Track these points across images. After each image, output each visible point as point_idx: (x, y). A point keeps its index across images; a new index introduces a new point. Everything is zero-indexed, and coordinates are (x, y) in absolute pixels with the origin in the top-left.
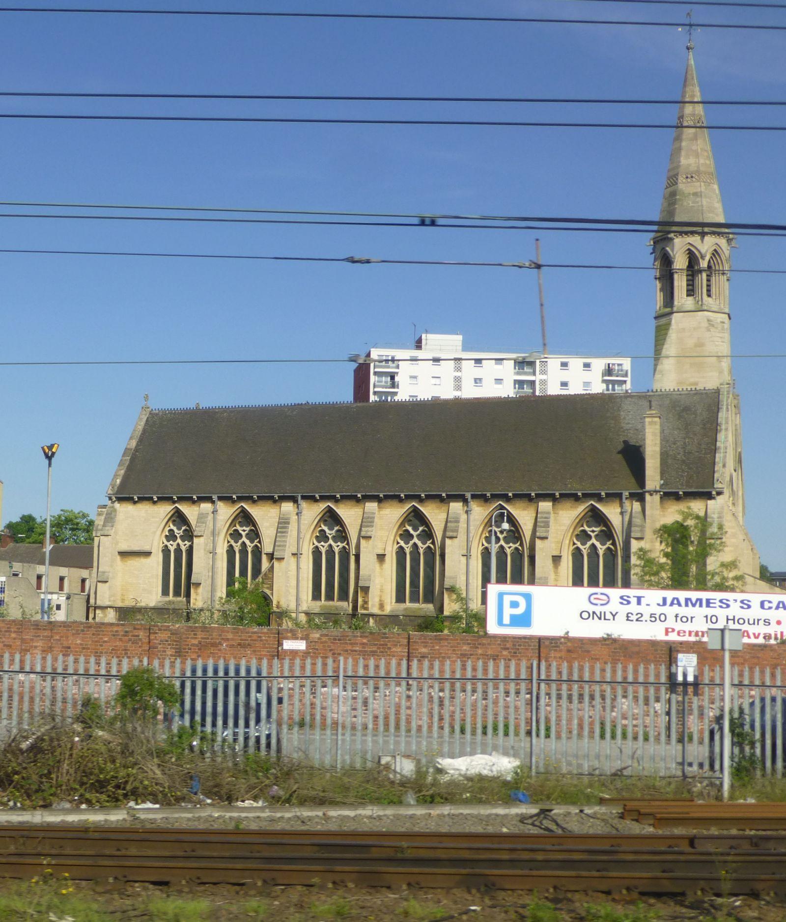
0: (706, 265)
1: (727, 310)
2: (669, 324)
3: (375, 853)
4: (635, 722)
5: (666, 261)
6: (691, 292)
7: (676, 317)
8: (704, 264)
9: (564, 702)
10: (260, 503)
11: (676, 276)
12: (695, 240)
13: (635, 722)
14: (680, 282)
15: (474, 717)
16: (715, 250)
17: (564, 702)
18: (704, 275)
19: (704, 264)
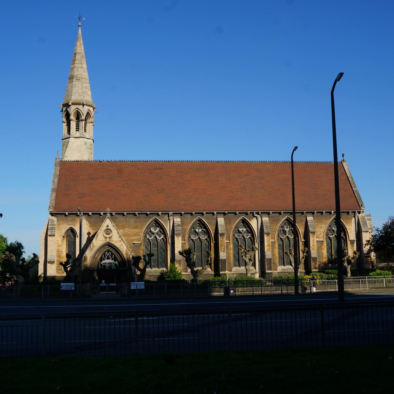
0: (84, 118)
1: (92, 138)
2: (68, 142)
3: (311, 288)
4: (367, 278)
5: (68, 115)
6: (78, 129)
7: (71, 140)
8: (83, 117)
9: (358, 284)
10: (70, 218)
11: (71, 122)
12: (80, 107)
13: (367, 278)
14: (73, 124)
15: (351, 286)
16: (88, 112)
17: (364, 284)
18: (83, 122)
19: (83, 117)
